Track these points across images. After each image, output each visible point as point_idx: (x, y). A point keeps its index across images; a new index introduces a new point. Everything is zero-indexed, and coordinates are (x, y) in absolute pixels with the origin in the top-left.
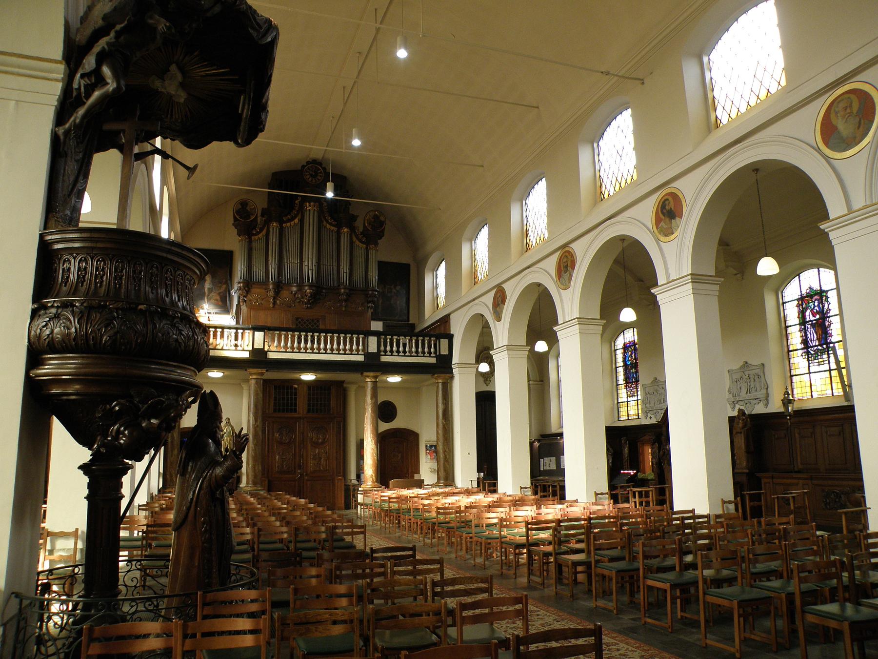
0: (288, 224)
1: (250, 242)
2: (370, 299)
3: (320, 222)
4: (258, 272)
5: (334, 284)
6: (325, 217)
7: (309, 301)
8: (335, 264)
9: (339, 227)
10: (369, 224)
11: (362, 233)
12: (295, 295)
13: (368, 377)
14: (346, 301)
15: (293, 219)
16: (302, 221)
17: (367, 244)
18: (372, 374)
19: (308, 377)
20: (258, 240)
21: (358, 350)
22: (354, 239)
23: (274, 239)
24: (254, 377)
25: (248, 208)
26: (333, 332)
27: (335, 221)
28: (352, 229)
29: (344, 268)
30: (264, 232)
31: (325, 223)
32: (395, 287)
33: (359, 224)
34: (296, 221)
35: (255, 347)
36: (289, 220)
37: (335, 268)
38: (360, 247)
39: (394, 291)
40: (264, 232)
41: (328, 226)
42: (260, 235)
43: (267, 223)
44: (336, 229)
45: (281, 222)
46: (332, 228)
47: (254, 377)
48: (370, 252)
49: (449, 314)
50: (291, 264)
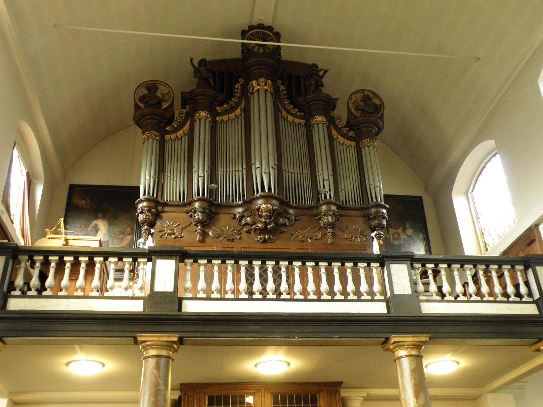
0: (225, 118)
1: (162, 143)
2: (375, 223)
3: (277, 111)
4: (174, 189)
5: (309, 201)
6: (283, 105)
7: (266, 224)
8: (307, 171)
9: (308, 116)
10: (357, 109)
11: (346, 126)
12: (240, 219)
13: (400, 345)
14: (332, 225)
15: (233, 109)
16: (247, 111)
17: (358, 139)
18: (409, 339)
19: (274, 363)
20: (177, 141)
21: (371, 292)
22: (334, 133)
23: (202, 135)
24: (153, 352)
25: (159, 94)
26: (317, 259)
27: (300, 111)
28: (331, 121)
29: (324, 174)
30: (187, 127)
31: (284, 113)
32: (404, 231)
33: (341, 113)
34: (238, 112)
35: (157, 289)
36: (226, 112)
37: (307, 177)
38: (346, 148)
39: (403, 236)
40: (187, 127)
41: (290, 118)
42: (180, 133)
43: (190, 116)
44: (303, 122)
45: (214, 114)
46: (297, 121)
47: (153, 352)
48: (365, 151)
49: (536, 226)
50: (232, 176)
